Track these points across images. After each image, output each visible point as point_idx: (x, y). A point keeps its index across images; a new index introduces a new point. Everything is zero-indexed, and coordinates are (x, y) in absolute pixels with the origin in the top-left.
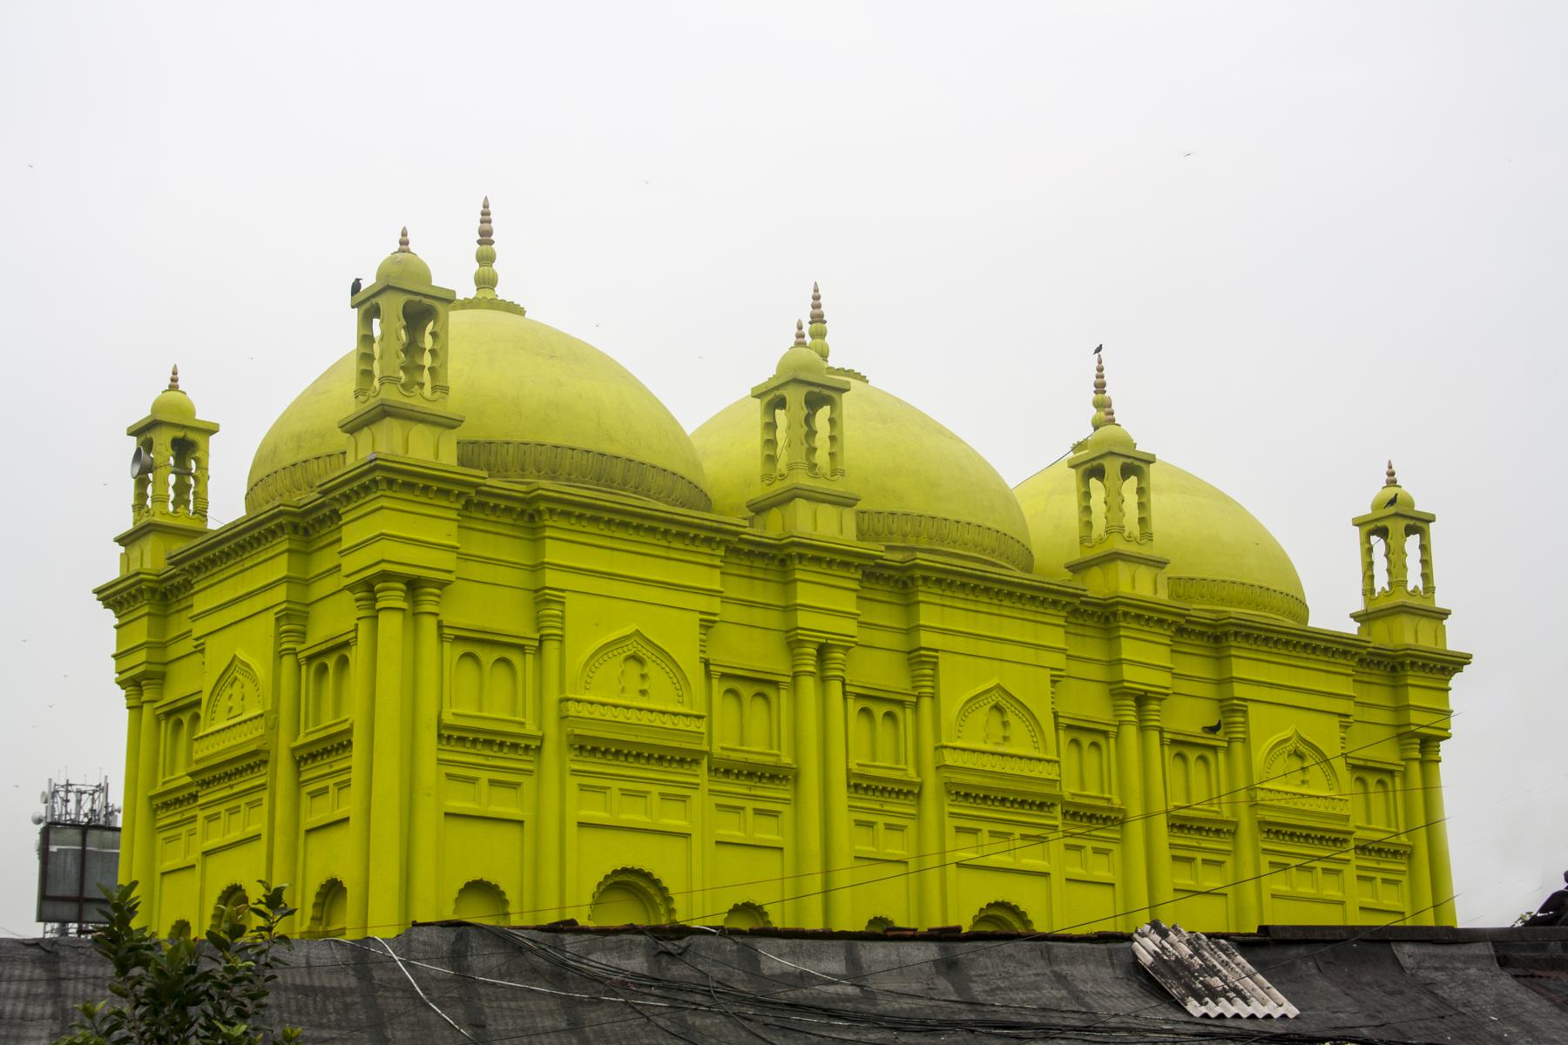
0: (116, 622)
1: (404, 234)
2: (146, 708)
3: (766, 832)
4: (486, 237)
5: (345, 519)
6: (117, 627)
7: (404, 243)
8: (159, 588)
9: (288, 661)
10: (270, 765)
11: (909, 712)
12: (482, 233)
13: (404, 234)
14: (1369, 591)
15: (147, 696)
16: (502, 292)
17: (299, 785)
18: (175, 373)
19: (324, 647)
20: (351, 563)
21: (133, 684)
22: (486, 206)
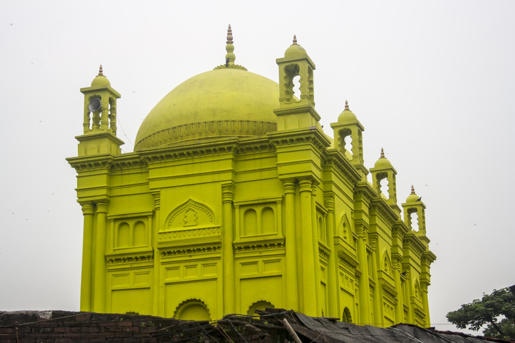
0: (77, 174)
1: (295, 38)
2: (100, 218)
3: (272, 270)
4: (230, 40)
5: (150, 167)
7: (295, 41)
8: (102, 166)
9: (228, 206)
10: (222, 249)
11: (279, 206)
12: (228, 39)
13: (295, 38)
14: (86, 125)
17: (235, 259)
18: (101, 68)
20: (282, 170)
21: (92, 206)
22: (230, 28)
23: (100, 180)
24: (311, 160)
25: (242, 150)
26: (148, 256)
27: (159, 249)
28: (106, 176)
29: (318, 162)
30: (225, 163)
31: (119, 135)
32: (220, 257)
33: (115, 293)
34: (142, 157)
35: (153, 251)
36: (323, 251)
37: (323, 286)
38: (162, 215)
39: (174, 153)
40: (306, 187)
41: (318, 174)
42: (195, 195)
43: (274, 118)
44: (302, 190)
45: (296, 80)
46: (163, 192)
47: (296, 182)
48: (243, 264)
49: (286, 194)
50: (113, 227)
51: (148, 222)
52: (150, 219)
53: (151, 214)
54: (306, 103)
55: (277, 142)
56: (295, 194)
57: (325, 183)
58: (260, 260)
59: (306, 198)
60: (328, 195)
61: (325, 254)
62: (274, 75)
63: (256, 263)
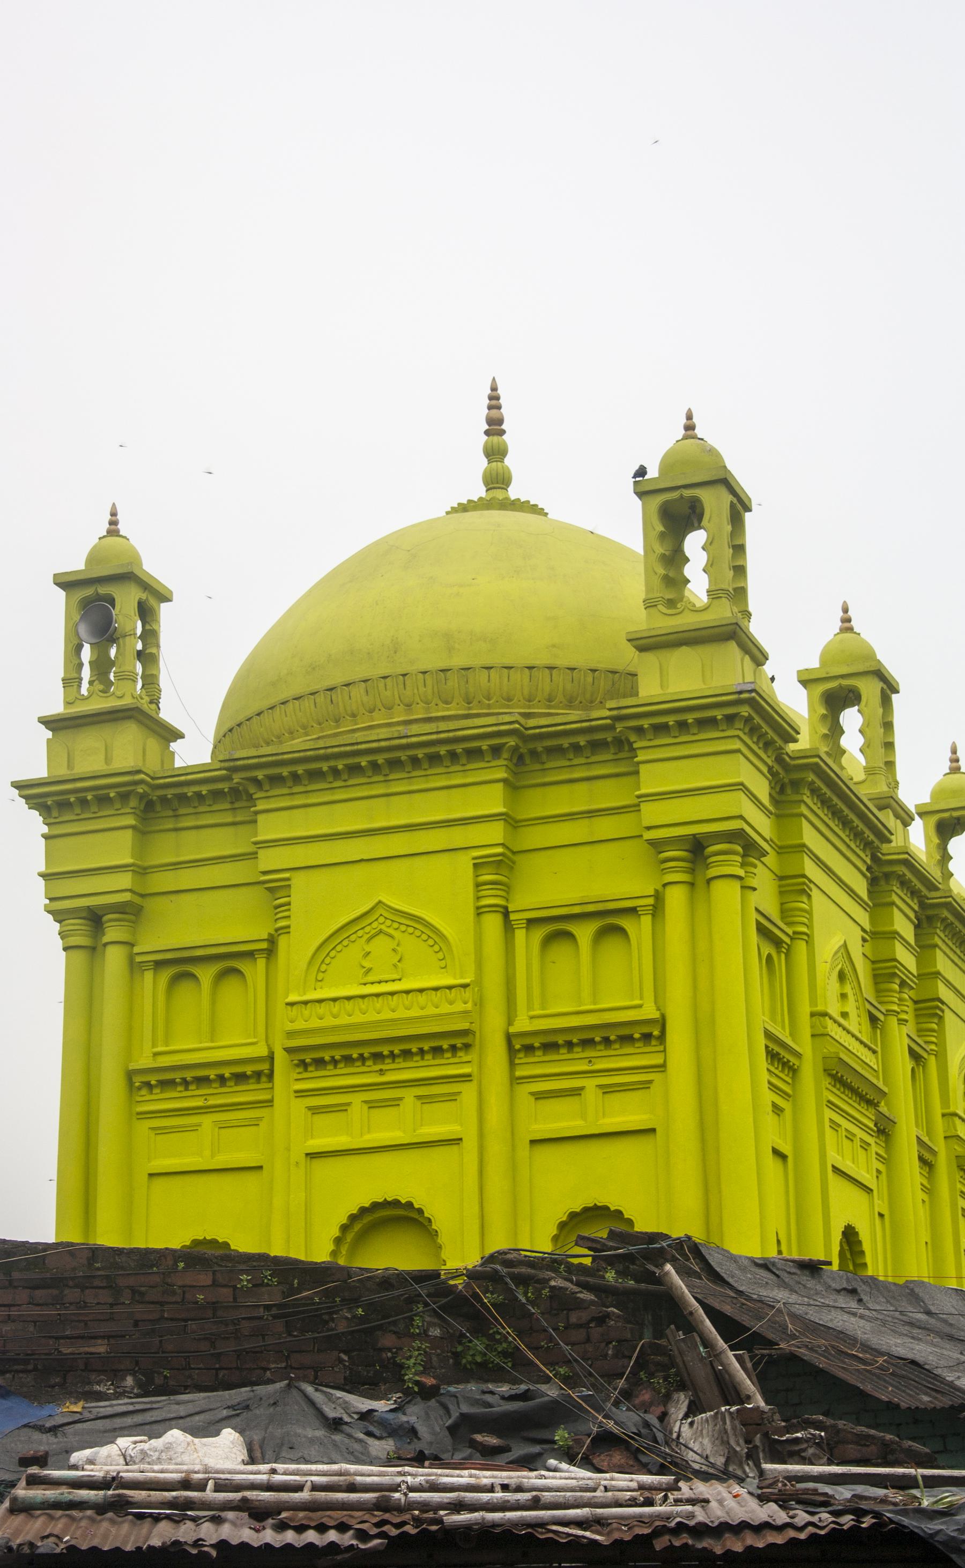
0: (45, 829)
1: (689, 417)
2: (114, 958)
3: (626, 1113)
4: (495, 426)
5: (261, 806)
6: (46, 837)
7: (690, 427)
9: (493, 923)
11: (646, 921)
12: (491, 398)
13: (689, 417)
15: (112, 933)
16: (514, 492)
17: (515, 1081)
18: (114, 514)
19: (577, 910)
21: (88, 924)
22: (494, 388)
23: (112, 842)
24: (742, 784)
25: (534, 753)
26: (256, 1073)
27: (289, 1050)
28: (129, 834)
29: (762, 788)
30: (484, 792)
31: (168, 713)
32: (469, 1075)
33: (159, 1183)
34: (237, 778)
35: (271, 1058)
36: (780, 1057)
37: (779, 1162)
38: (296, 951)
39: (332, 763)
40: (728, 863)
41: (761, 824)
42: (396, 889)
43: (628, 657)
44: (712, 872)
45: (694, 543)
46: (299, 881)
47: (697, 849)
48: (539, 1096)
49: (665, 885)
50: (152, 984)
51: (256, 971)
52: (261, 963)
53: (264, 945)
54: (724, 612)
55: (640, 730)
56: (692, 884)
57: (782, 850)
58: (590, 1084)
59: (726, 895)
60: (793, 887)
61: (785, 1065)
62: (626, 525)
63: (576, 1092)
